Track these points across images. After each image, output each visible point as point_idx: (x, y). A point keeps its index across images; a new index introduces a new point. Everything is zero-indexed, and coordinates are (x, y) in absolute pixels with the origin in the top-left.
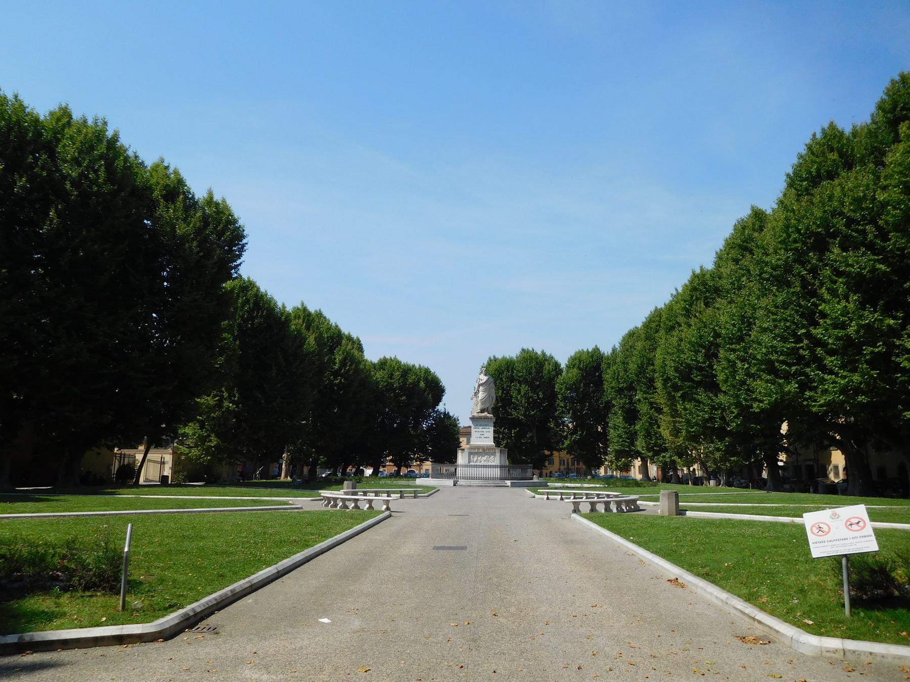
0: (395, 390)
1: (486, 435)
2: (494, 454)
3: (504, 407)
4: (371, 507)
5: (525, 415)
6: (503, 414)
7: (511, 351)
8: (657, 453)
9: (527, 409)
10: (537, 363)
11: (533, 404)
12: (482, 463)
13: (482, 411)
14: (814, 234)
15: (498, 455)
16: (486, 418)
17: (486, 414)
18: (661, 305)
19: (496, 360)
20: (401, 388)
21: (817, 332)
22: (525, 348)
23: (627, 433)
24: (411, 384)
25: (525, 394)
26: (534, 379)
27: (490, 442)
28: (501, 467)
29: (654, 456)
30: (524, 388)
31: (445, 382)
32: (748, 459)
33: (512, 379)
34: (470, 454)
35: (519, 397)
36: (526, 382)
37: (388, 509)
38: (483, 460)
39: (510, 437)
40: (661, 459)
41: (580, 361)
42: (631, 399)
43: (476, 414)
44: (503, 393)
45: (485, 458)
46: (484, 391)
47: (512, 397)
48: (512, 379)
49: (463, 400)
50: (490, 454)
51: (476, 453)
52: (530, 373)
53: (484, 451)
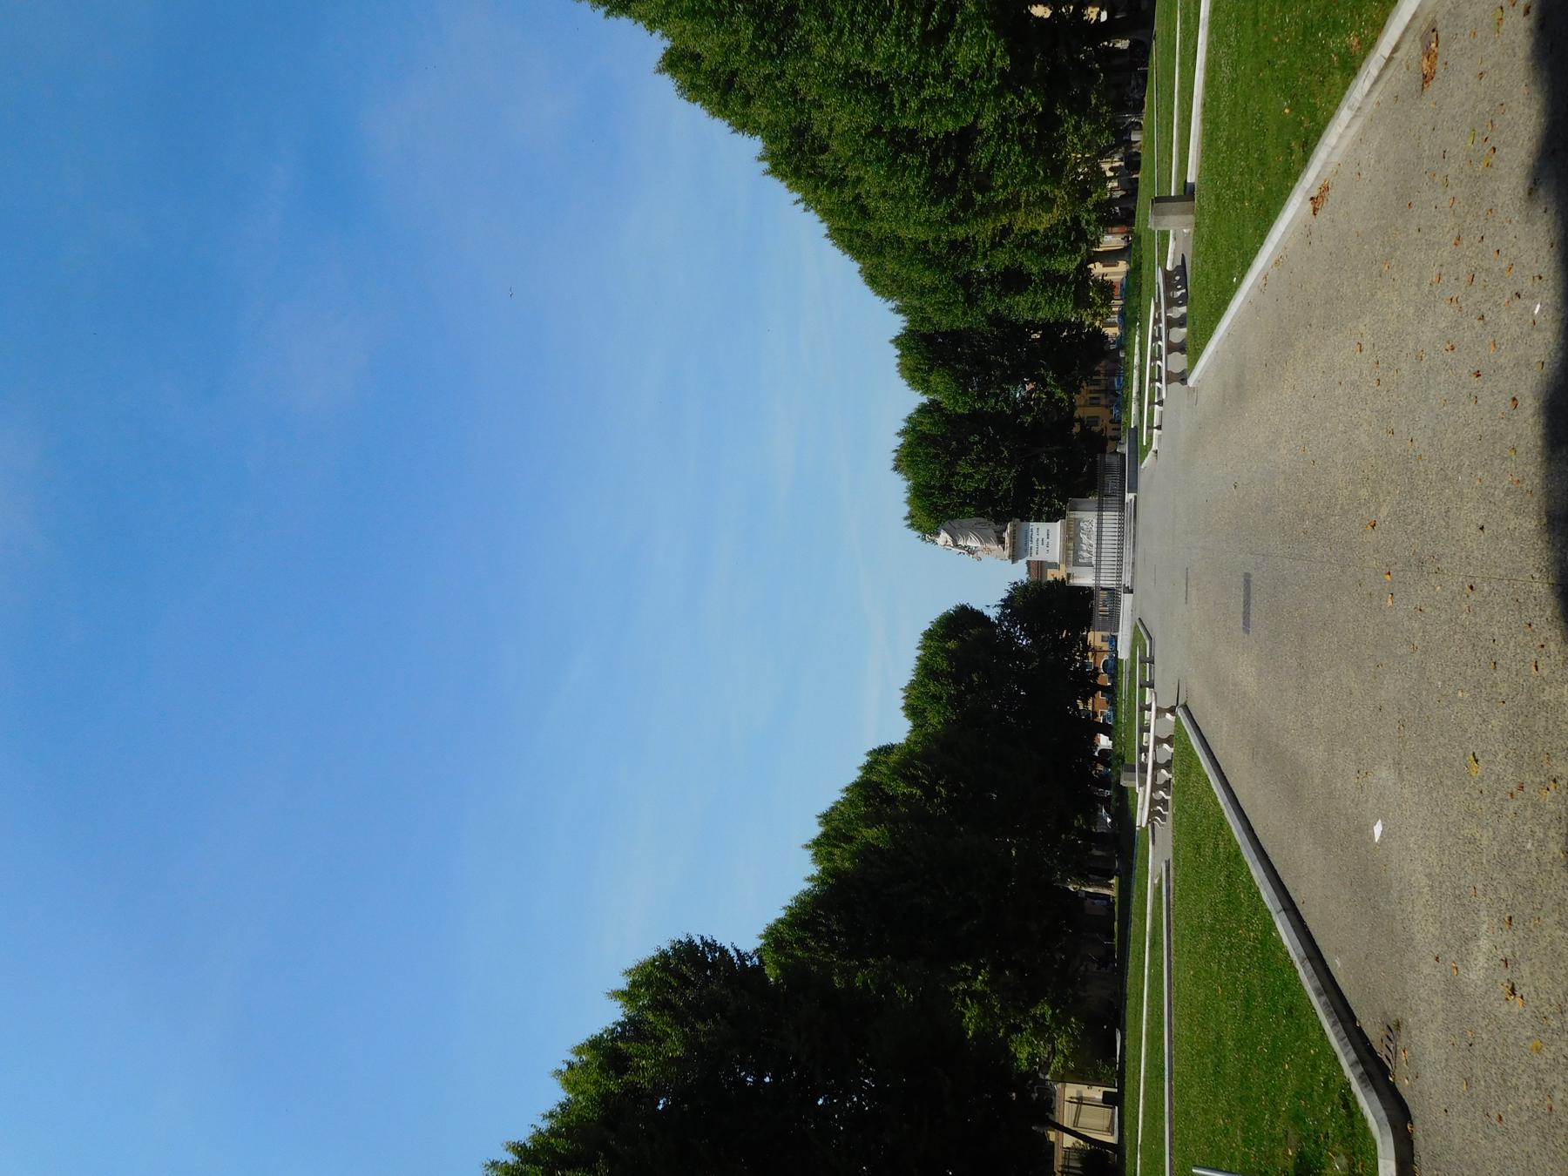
1: (1043, 534)
2: (1077, 522)
5: (1010, 467)
8: (1082, 235)
10: (919, 445)
12: (1094, 542)
13: (1001, 541)
15: (1079, 515)
16: (1013, 536)
17: (1006, 535)
18: (823, 228)
19: (911, 516)
20: (957, 683)
22: (892, 464)
23: (1045, 287)
24: (950, 665)
25: (973, 465)
27: (1056, 528)
29: (1087, 241)
30: (963, 467)
33: (946, 489)
34: (1076, 563)
35: (977, 477)
36: (951, 465)
38: (1088, 541)
39: (1048, 493)
40: (1092, 228)
43: (1007, 553)
44: (969, 505)
45: (1084, 537)
46: (966, 537)
47: (977, 489)
48: (946, 489)
51: (1076, 553)
52: (937, 456)
53: (1071, 540)
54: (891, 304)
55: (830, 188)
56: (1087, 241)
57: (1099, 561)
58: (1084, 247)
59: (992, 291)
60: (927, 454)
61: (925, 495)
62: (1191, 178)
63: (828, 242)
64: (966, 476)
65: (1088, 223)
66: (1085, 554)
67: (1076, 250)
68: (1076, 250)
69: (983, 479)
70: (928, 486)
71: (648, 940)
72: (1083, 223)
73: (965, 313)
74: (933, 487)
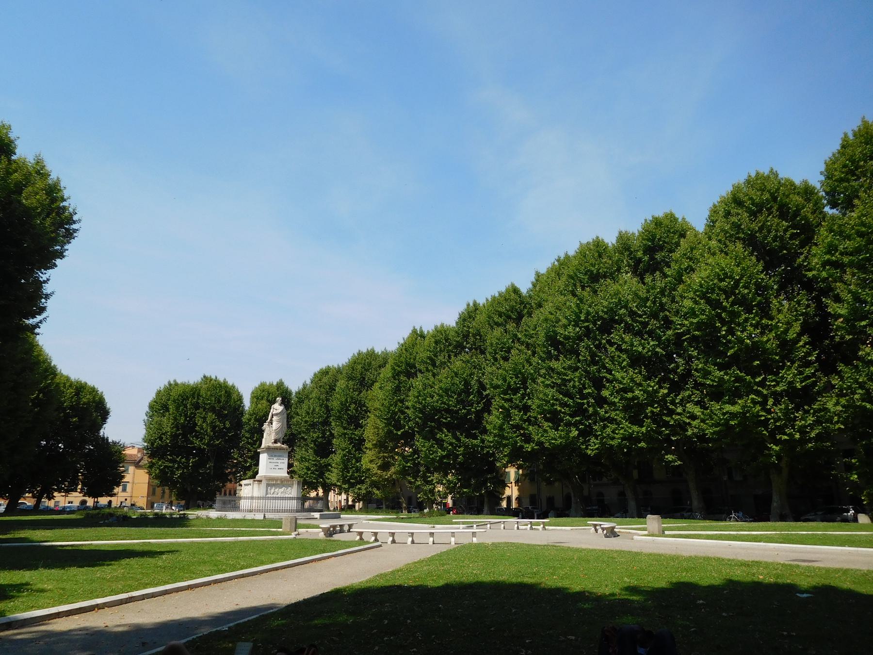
0: (65, 409)
1: (281, 466)
2: (291, 486)
3: (184, 435)
4: (361, 539)
5: (208, 445)
6: (182, 442)
7: (191, 377)
8: (352, 485)
9: (211, 439)
10: (226, 392)
11: (218, 433)
12: (279, 495)
13: (275, 442)
14: (601, 318)
15: (295, 486)
16: (281, 449)
17: (279, 445)
18: (379, 350)
19: (176, 384)
20: (72, 407)
21: (605, 393)
22: (208, 375)
23: (316, 465)
24: (84, 404)
25: (212, 422)
26: (223, 408)
27: (284, 473)
28: (298, 499)
29: (349, 488)
30: (211, 416)
31: (110, 403)
32: (480, 490)
33: (197, 406)
34: (268, 485)
35: (204, 425)
36: (213, 410)
37: (376, 540)
38: (280, 492)
39: (187, 467)
40: (356, 491)
41: (269, 394)
42: (324, 433)
43: (270, 445)
44: (185, 420)
45: (282, 490)
46: (279, 421)
47: (196, 424)
48: (197, 406)
49: (127, 427)
50: (287, 486)
51: (274, 485)
52: (219, 402)
53: (273, 483)
54: (308, 382)
55: (430, 358)
56: (349, 488)
57: (269, 498)
58: (346, 486)
59: (318, 437)
60: (221, 396)
61: (194, 393)
62: (635, 537)
63: (356, 352)
64: (204, 418)
65: (360, 489)
66: (273, 491)
67: (344, 482)
68: (344, 482)
69: (202, 428)
70: (199, 395)
71: (77, 197)
72: (359, 486)
73: (306, 422)
74: (198, 399)
